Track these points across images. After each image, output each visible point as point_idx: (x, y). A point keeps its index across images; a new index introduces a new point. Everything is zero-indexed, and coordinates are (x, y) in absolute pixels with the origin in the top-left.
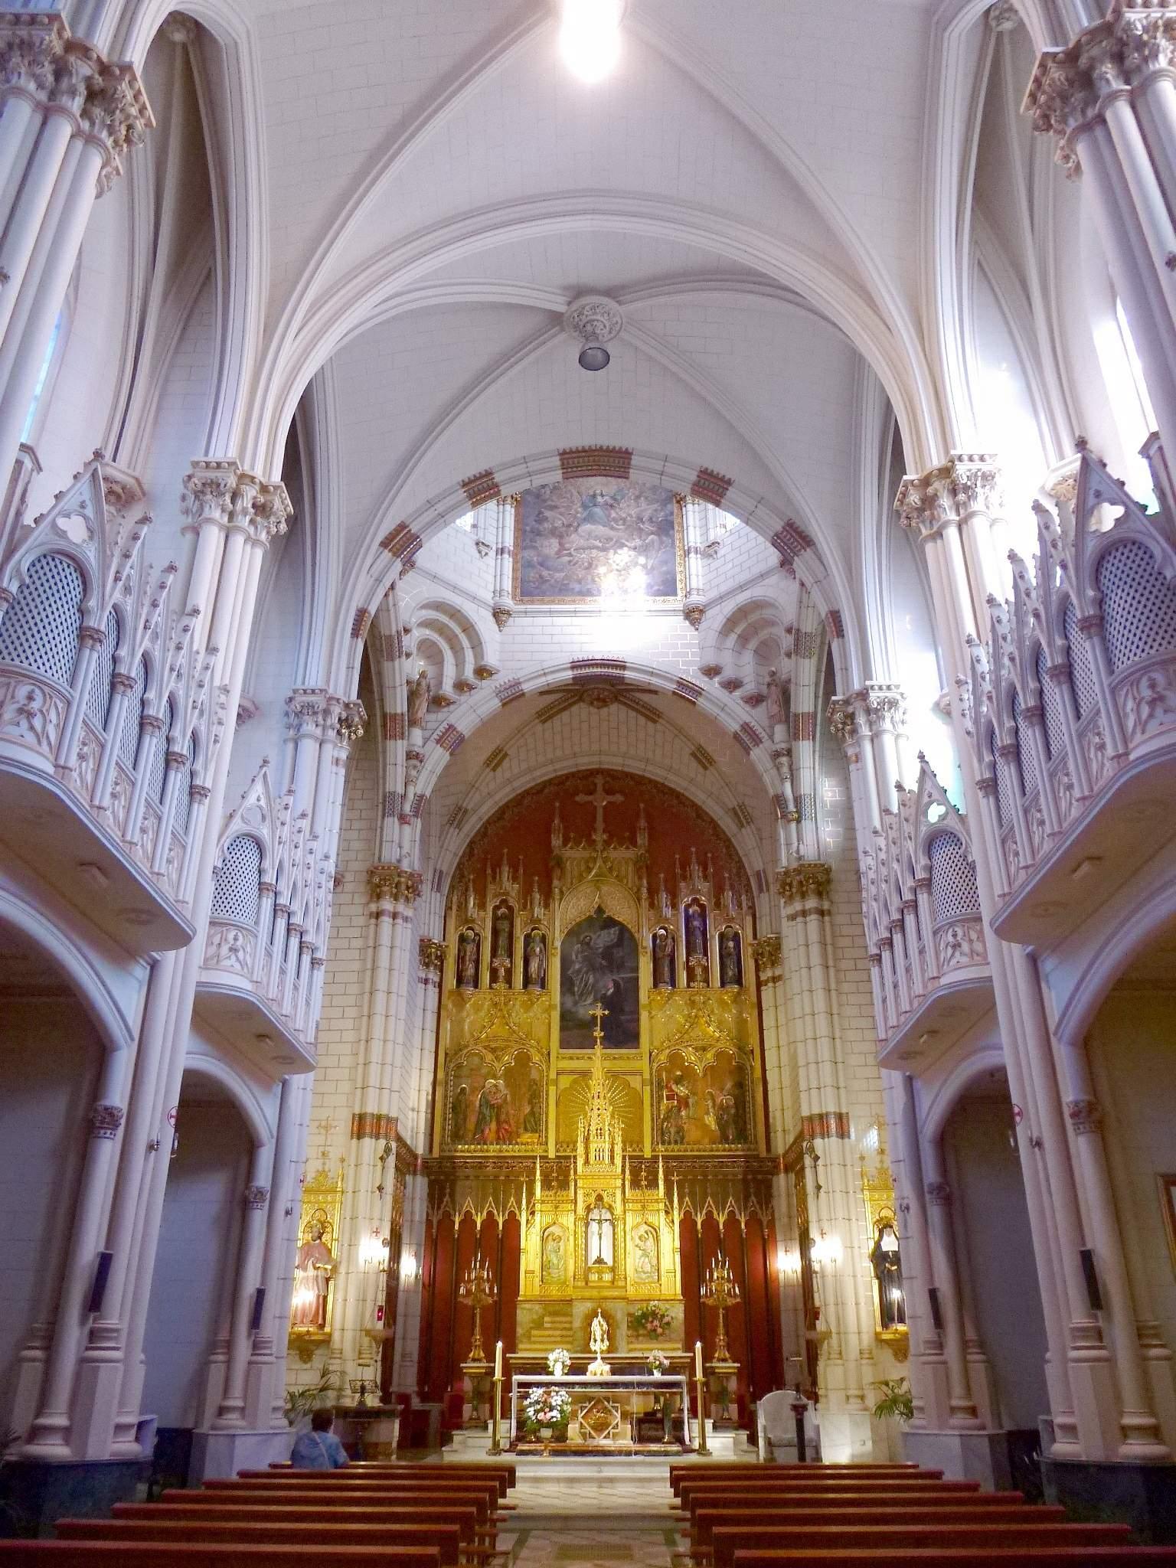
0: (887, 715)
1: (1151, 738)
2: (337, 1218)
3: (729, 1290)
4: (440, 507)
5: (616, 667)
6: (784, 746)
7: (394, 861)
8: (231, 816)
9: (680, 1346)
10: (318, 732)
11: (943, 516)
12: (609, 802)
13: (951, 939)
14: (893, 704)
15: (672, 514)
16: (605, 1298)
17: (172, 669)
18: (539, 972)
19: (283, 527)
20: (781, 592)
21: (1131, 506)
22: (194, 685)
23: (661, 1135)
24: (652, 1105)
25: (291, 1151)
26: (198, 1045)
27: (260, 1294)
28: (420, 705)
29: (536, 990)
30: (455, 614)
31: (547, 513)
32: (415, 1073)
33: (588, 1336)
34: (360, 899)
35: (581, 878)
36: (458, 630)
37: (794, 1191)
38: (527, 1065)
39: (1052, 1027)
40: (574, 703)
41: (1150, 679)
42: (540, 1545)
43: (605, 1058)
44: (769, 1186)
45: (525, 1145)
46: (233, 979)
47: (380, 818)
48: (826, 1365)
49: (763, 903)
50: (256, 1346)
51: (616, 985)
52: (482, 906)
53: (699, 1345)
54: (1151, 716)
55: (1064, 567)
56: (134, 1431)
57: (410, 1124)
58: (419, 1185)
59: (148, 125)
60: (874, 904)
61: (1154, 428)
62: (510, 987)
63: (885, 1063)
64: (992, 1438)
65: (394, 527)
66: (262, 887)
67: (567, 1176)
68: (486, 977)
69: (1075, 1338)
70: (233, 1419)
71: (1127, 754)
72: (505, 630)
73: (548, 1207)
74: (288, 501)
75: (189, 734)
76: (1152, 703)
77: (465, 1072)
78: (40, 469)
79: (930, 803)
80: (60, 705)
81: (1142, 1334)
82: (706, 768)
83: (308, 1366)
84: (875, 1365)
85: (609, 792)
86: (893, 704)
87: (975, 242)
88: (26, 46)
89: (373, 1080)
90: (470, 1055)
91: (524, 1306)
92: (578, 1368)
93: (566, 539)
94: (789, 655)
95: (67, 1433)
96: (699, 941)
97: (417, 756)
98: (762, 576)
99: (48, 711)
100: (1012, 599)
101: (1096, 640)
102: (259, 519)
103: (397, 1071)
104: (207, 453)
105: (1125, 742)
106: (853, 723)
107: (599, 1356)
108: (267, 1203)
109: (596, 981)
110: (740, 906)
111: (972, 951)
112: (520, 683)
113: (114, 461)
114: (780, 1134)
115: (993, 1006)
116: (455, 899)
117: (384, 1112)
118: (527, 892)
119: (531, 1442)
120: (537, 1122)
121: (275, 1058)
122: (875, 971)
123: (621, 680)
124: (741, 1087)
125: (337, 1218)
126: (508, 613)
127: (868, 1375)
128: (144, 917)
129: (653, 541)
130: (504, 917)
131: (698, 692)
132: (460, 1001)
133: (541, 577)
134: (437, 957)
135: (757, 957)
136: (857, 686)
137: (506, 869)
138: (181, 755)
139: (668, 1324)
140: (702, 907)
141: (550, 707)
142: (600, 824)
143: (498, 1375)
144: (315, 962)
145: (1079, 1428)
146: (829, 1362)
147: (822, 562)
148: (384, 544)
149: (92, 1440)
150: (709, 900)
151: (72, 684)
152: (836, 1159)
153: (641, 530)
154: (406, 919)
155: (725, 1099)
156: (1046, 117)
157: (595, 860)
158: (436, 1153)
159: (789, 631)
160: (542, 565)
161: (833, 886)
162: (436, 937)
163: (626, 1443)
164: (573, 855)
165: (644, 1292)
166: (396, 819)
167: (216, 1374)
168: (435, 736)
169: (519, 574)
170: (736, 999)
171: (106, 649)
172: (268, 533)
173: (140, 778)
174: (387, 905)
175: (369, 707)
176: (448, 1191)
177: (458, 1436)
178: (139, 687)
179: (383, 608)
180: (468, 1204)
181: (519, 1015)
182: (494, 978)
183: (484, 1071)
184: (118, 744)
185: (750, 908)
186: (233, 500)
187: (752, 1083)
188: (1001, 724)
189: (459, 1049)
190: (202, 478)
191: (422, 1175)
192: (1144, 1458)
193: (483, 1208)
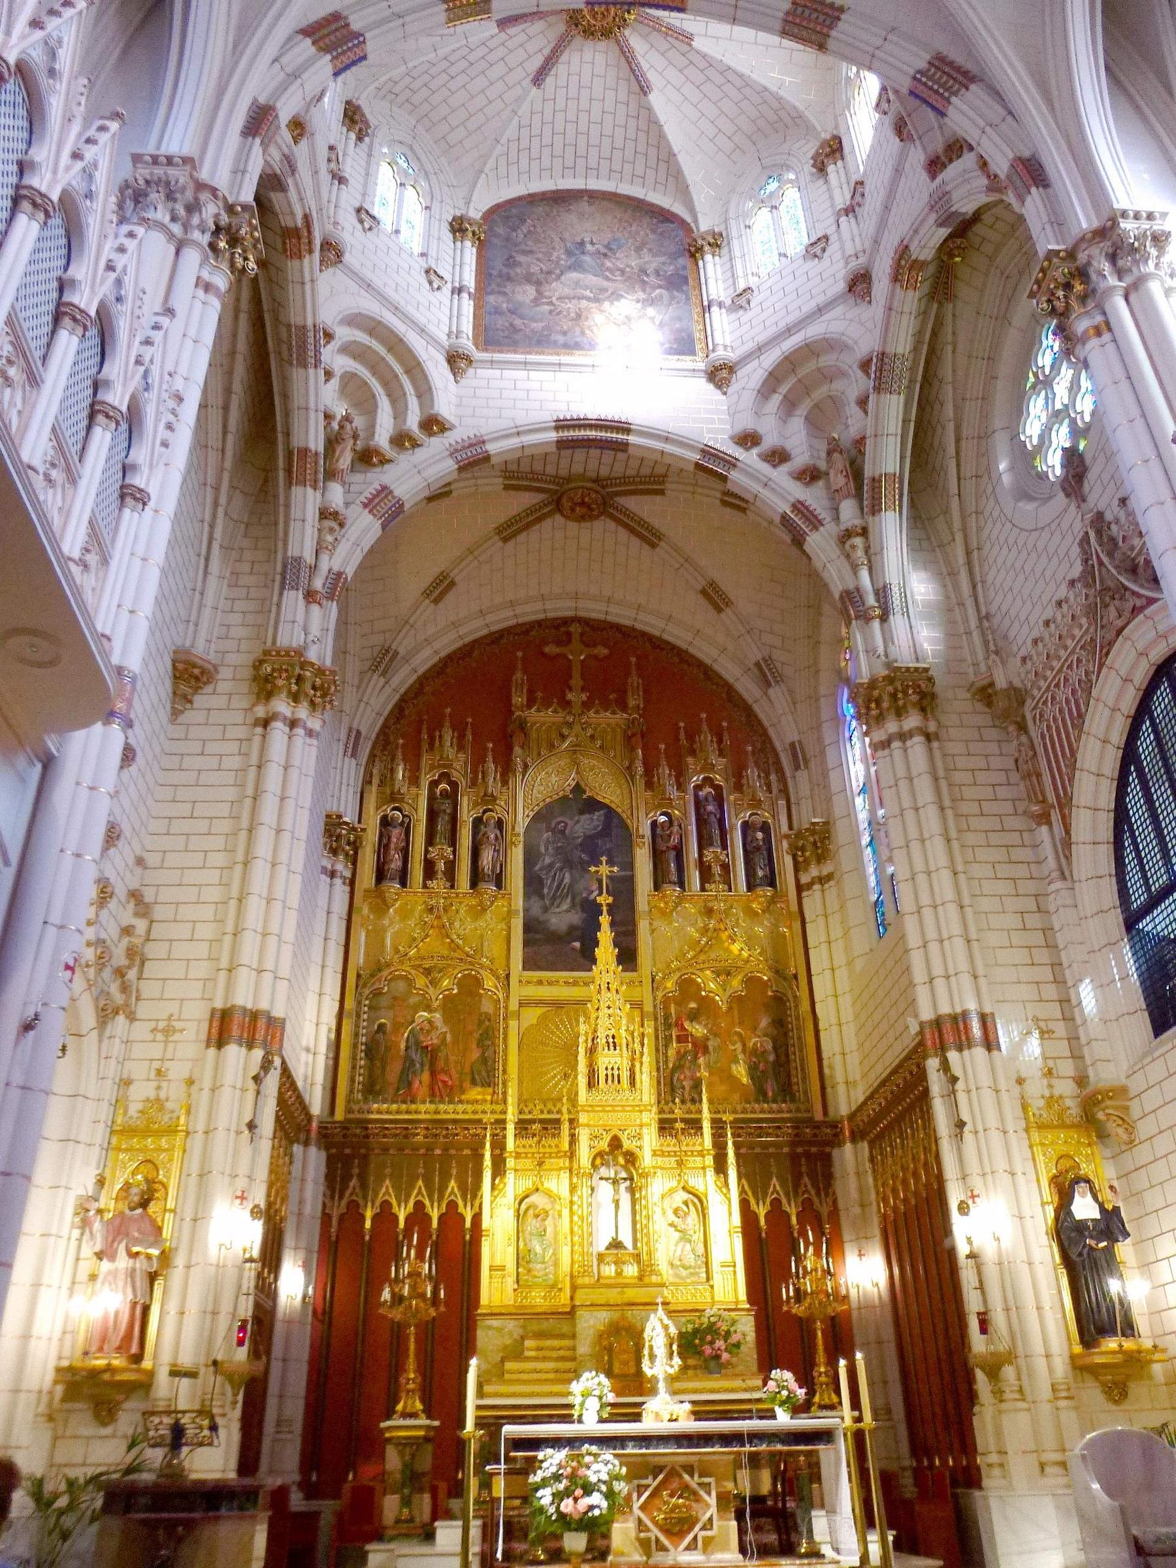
2: (175, 1172)
18: (494, 867)
28: (342, 452)
30: (396, 344)
31: (521, 258)
32: (312, 999)
36: (398, 368)
44: (826, 1160)
52: (414, 780)
62: (452, 887)
72: (463, 382)
73: (528, 1163)
77: (384, 1001)
83: (107, 1431)
84: (1076, 1408)
91: (489, 1323)
97: (335, 515)
98: (820, 310)
110: (769, 786)
114: (841, 1089)
117: (264, 1005)
118: (478, 761)
125: (175, 1172)
130: (444, 794)
131: (732, 463)
132: (381, 905)
140: (718, 788)
142: (576, 681)
146: (1003, 1406)
150: (727, 780)
152: (985, 1080)
154: (310, 733)
157: (570, 725)
158: (339, 1115)
160: (512, 312)
162: (349, 812)
164: (541, 718)
166: (301, 596)
174: (282, 706)
176: (356, 1171)
181: (464, 925)
182: (429, 870)
183: (413, 1000)
187: (797, 1019)
189: (377, 968)
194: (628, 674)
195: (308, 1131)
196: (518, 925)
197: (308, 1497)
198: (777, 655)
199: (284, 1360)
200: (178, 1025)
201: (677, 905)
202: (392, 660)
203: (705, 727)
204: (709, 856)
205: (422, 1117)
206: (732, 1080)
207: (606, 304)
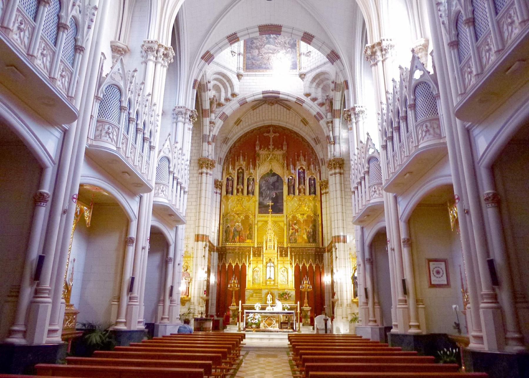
0: (360, 115)
1: (425, 142)
2: (191, 265)
4: (220, 45)
5: (277, 93)
6: (330, 120)
8: (160, 151)
11: (378, 58)
13: (374, 190)
14: (362, 112)
17: (144, 113)
19: (172, 60)
20: (330, 69)
21: (426, 72)
23: (290, 240)
26: (154, 218)
27: (172, 287)
29: (251, 195)
30: (224, 76)
33: (266, 300)
38: (248, 219)
39: (399, 217)
40: (264, 104)
41: (426, 125)
44: (322, 256)
45: (248, 243)
46: (162, 200)
49: (324, 168)
50: (171, 301)
51: (276, 194)
53: (298, 303)
54: (425, 136)
55: (406, 87)
58: (215, 255)
63: (355, 223)
64: (380, 329)
65: (205, 52)
67: (260, 253)
69: (399, 302)
70: (166, 321)
71: (418, 146)
72: (241, 81)
73: (255, 262)
74: (174, 52)
76: (426, 132)
77: (229, 221)
78: (106, 58)
80: (116, 130)
81: (417, 301)
83: (184, 307)
85: (275, 133)
86: (362, 112)
89: (201, 224)
92: (263, 308)
93: (261, 50)
94: (333, 91)
96: (302, 180)
97: (213, 123)
98: (325, 64)
101: (413, 111)
104: (148, 38)
107: (269, 305)
110: (316, 169)
113: (119, 40)
114: (326, 241)
116: (225, 167)
117: (205, 234)
118: (248, 165)
120: (251, 236)
122: (353, 196)
124: (315, 227)
125: (191, 265)
126: (242, 75)
127: (349, 311)
129: (289, 51)
130: (241, 172)
131: (303, 102)
132: (227, 199)
135: (321, 185)
136: (352, 106)
137: (241, 157)
139: (290, 296)
140: (304, 170)
141: (256, 105)
142: (271, 143)
143: (240, 310)
145: (398, 326)
147: (342, 63)
148: (202, 58)
149: (37, 335)
154: (210, 175)
155: (310, 230)
157: (270, 155)
158: (220, 246)
159: (333, 82)
160: (252, 58)
161: (344, 165)
163: (277, 329)
164: (263, 153)
165: (283, 287)
167: (160, 308)
168: (219, 116)
170: (314, 199)
171: (126, 112)
173: (137, 146)
174: (204, 170)
176: (224, 257)
177: (228, 327)
180: (230, 261)
183: (235, 220)
185: (319, 170)
188: (388, 129)
191: (216, 252)
193: (235, 262)
195: (214, 249)
197: (217, 317)
198: (320, 137)
202: (228, 140)
206: (303, 238)
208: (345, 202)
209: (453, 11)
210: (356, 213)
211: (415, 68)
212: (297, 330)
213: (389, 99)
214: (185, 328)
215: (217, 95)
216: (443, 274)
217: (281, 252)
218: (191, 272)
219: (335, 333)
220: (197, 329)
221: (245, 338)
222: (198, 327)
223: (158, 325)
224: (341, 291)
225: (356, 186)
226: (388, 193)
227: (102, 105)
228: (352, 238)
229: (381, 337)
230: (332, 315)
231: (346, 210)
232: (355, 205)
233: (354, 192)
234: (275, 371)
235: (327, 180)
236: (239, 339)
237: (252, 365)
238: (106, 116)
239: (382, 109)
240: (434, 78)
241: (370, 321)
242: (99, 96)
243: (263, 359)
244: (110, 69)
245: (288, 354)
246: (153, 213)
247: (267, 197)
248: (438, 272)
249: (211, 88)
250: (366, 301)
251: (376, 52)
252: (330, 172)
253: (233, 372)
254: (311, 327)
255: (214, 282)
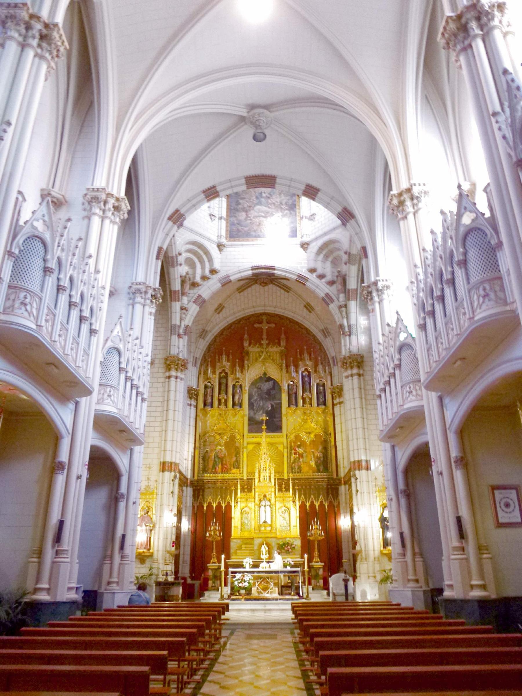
0: (385, 292)
2: (154, 505)
3: (319, 534)
4: (194, 202)
6: (343, 303)
7: (176, 354)
8: (107, 340)
9: (299, 556)
10: (142, 301)
12: (269, 327)
13: (408, 389)
14: (388, 287)
15: (295, 201)
16: (268, 537)
17: (82, 282)
19: (126, 216)
22: (90, 287)
23: (292, 469)
24: (288, 457)
25: (135, 478)
26: (96, 435)
27: (124, 536)
30: (201, 246)
31: (241, 201)
32: (186, 444)
33: (260, 552)
34: (162, 370)
35: (256, 359)
37: (348, 492)
39: (447, 427)
42: (240, 635)
43: (267, 437)
44: (337, 490)
45: (234, 474)
46: (109, 408)
47: (169, 335)
48: (360, 564)
49: (335, 370)
50: (122, 557)
51: (272, 406)
52: (214, 372)
53: (306, 556)
54: (483, 302)
55: (451, 238)
56: (75, 590)
57: (184, 466)
58: (189, 491)
59: (65, 49)
60: (378, 373)
61: (489, 182)
62: (227, 407)
63: (383, 440)
64: (425, 592)
66: (121, 369)
67: (251, 487)
68: (216, 403)
70: (114, 586)
71: (473, 318)
72: (223, 253)
74: (128, 205)
75: (89, 308)
76: (484, 297)
77: (208, 443)
79: (400, 332)
80: (37, 300)
81: (480, 549)
82: (310, 312)
83: (143, 566)
85: (268, 323)
86: (388, 287)
87: (424, 87)
88: (13, 17)
89: (169, 447)
90: (210, 436)
94: (346, 264)
95: (48, 590)
96: (308, 387)
98: (334, 229)
99: (33, 303)
100: (432, 250)
101: (463, 270)
102: (115, 213)
103: (179, 444)
104: (92, 185)
105: (473, 312)
106: (371, 295)
108: (125, 500)
109: (263, 404)
110: (325, 372)
111: (417, 395)
112: (229, 276)
115: (424, 418)
116: (202, 370)
117: (173, 461)
118: (233, 366)
119: (237, 595)
121: (127, 440)
122: (378, 402)
123: (273, 274)
124: (325, 449)
125: (154, 505)
126: (224, 246)
127: (377, 567)
128: (73, 384)
131: (306, 279)
132: (205, 414)
133: (238, 229)
134: (195, 395)
136: (373, 279)
138: (86, 317)
139: (294, 547)
140: (309, 372)
141: (243, 286)
142: (265, 336)
143: (223, 568)
144: (143, 400)
145: (454, 586)
148: (170, 219)
151: (42, 290)
153: (281, 208)
154: (181, 379)
156: (448, 43)
157: (262, 352)
158: (196, 478)
159: (346, 253)
160: (238, 224)
163: (276, 595)
164: (254, 350)
169: (229, 228)
170: (324, 412)
171: (54, 276)
172: (120, 218)
173: (70, 327)
175: (164, 291)
176: (201, 493)
177: (207, 594)
178: (68, 291)
179: (170, 245)
180: (209, 499)
183: (216, 443)
184: (61, 314)
186: (105, 205)
188: (427, 301)
189: (205, 434)
190: (91, 195)
192: (479, 597)
193: (216, 501)
194: (281, 334)
195: (187, 484)
196: (246, 419)
198: (329, 327)
199: (230, 182)
200: (152, 466)
201: (295, 411)
203: (305, 352)
204: (305, 396)
205: (220, 478)
207: (269, 218)
208: (367, 414)
209: (518, 117)
210: (383, 426)
211: (463, 210)
212: (305, 597)
213: (427, 259)
214: (140, 596)
215: (191, 272)
216: (515, 507)
217: (280, 485)
218: (154, 515)
219: (359, 599)
220: (162, 598)
221: (228, 610)
222: (161, 594)
223: (102, 593)
224: (364, 539)
225: (383, 387)
226: (429, 392)
227: (17, 264)
228: (377, 464)
229: (426, 606)
230: (353, 574)
231: (368, 425)
232: (382, 414)
233: (380, 396)
234: (272, 660)
235: (342, 386)
236: (219, 611)
237: (237, 652)
238: (22, 280)
239: (417, 275)
240: (493, 222)
241: (409, 580)
242: (13, 251)
243: (256, 641)
244: (31, 215)
245: (292, 633)
246: (94, 426)
247: (260, 410)
248: (507, 505)
249: (183, 262)
250: (402, 552)
251: (404, 201)
252: (345, 374)
253: (209, 665)
254: (325, 592)
255: (187, 530)
